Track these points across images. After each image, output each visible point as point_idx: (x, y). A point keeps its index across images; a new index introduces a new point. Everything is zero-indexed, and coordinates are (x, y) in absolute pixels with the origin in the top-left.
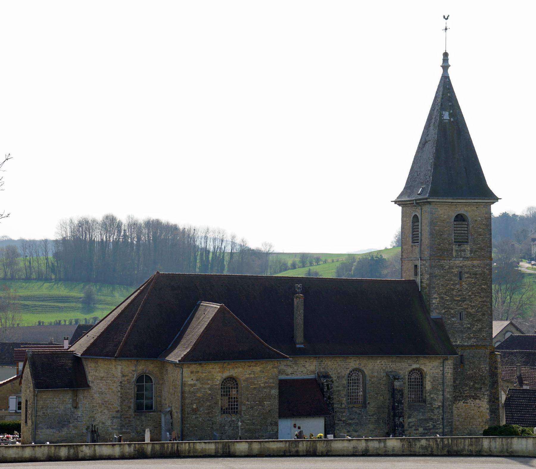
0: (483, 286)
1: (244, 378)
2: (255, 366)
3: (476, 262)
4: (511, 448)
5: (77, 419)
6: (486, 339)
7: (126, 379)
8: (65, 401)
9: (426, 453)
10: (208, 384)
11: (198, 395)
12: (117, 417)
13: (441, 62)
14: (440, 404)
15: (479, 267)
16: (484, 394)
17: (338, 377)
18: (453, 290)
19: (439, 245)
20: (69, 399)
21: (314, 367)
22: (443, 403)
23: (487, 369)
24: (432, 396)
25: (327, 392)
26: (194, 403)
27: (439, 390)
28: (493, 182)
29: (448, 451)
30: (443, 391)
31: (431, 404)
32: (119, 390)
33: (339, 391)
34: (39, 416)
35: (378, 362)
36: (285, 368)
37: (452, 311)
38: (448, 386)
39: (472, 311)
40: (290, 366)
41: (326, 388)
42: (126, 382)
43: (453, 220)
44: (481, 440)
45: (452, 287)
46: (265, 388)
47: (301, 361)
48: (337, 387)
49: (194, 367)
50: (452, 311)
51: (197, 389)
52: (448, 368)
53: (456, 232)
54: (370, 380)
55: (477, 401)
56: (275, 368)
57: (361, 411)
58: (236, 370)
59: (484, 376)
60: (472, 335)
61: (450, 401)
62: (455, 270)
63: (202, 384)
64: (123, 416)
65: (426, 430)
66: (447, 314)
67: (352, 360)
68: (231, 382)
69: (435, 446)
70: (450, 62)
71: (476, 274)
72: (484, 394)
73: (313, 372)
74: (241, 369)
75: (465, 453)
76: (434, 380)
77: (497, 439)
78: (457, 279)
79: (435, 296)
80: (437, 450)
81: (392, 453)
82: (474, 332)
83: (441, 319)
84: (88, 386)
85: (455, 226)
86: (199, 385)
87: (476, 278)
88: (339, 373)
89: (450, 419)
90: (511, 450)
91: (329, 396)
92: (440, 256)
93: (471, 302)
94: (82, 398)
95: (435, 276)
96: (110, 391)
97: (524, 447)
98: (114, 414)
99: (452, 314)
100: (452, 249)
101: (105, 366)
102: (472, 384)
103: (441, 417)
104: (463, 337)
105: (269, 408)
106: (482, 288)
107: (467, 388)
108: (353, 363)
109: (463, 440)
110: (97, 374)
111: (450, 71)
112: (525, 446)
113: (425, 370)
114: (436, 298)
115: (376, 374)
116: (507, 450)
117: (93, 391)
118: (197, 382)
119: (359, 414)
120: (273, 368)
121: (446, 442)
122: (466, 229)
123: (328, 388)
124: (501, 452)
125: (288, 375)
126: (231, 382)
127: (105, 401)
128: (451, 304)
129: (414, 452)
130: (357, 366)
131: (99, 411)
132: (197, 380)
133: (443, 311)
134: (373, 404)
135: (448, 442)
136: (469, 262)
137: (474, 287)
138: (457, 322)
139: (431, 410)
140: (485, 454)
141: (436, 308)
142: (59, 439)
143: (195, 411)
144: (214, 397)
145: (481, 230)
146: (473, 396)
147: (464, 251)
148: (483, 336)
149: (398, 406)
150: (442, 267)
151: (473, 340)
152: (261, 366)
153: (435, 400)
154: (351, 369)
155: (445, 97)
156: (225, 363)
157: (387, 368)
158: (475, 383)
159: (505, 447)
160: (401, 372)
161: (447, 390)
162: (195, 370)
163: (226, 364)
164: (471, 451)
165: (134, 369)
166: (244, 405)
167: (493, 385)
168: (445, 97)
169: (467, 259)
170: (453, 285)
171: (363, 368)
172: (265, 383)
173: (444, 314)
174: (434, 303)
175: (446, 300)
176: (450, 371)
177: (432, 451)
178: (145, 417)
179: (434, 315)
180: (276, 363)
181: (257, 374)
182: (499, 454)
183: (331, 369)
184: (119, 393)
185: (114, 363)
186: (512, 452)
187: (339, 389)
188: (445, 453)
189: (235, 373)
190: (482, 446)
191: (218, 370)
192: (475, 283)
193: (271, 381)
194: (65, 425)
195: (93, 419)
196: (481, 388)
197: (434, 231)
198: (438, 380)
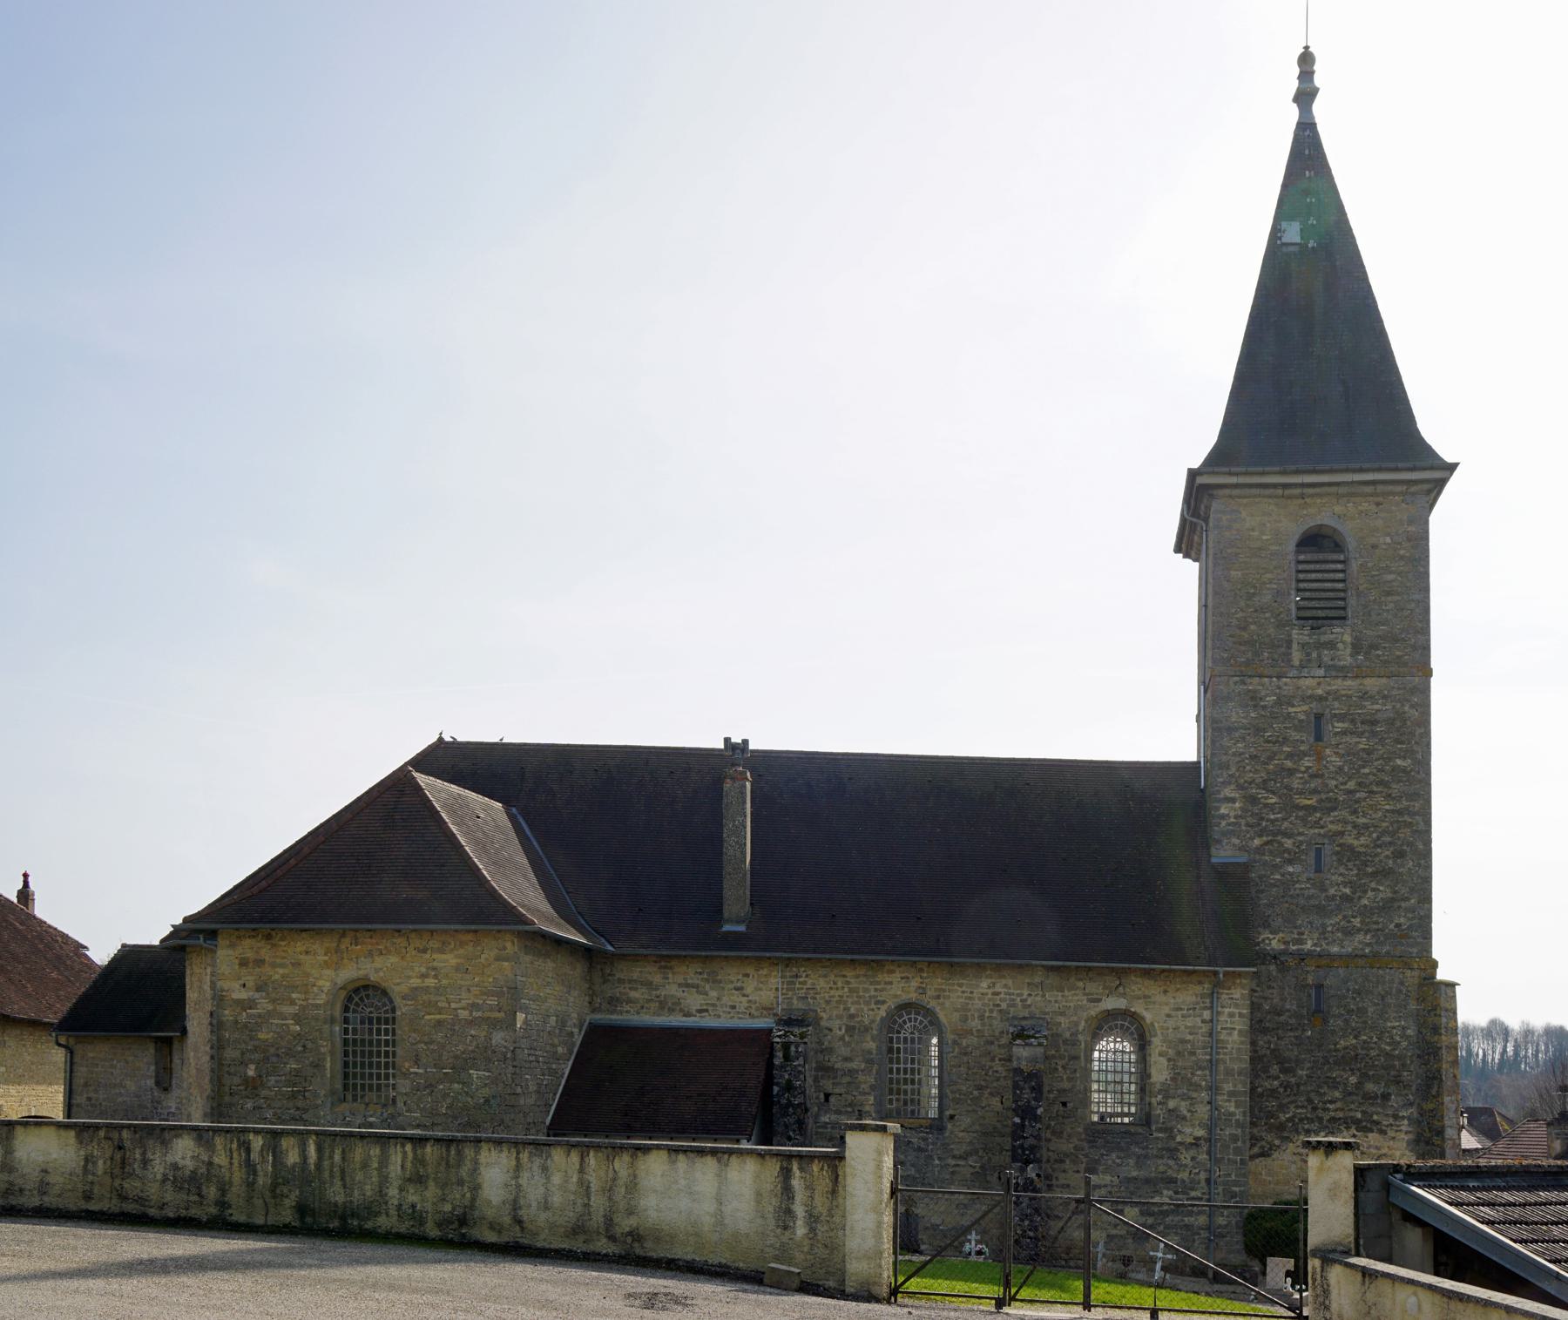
0: (1399, 762)
1: (404, 988)
2: (442, 951)
3: (1371, 684)
4: (630, 1212)
6: (1406, 936)
9: (194, 1212)
10: (293, 1003)
11: (262, 1036)
13: (1293, 85)
14: (1200, 1133)
15: (1385, 697)
16: (1396, 1117)
17: (850, 1029)
18: (1291, 772)
19: (1244, 629)
21: (771, 994)
22: (1210, 1130)
23: (1409, 1032)
24: (1171, 1104)
25: (782, 1067)
26: (251, 1061)
27: (1197, 1087)
28: (1436, 423)
29: (302, 1209)
30: (1214, 1089)
31: (1168, 1130)
33: (852, 1072)
35: (984, 985)
36: (679, 994)
37: (1288, 843)
38: (1229, 1072)
39: (1360, 843)
40: (697, 987)
41: (780, 1054)
43: (1292, 547)
44: (469, 1152)
45: (1289, 764)
46: (471, 1023)
47: (731, 974)
48: (846, 1059)
49: (249, 947)
50: (1288, 843)
51: (260, 1016)
52: (1231, 1015)
53: (1302, 585)
54: (955, 1042)
55: (1373, 1137)
56: (507, 959)
57: (925, 1139)
58: (379, 962)
59: (1399, 1057)
60: (1357, 922)
61: (1238, 1124)
62: (1299, 710)
63: (274, 1001)
65: (1151, 1214)
66: (1271, 852)
67: (896, 977)
68: (362, 996)
69: (238, 1176)
70: (1318, 80)
71: (1374, 723)
72: (1396, 1117)
73: (767, 1010)
74: (394, 959)
75: (383, 1223)
76: (1179, 1053)
77: (558, 1155)
78: (1305, 738)
79: (1228, 792)
80: (249, 1200)
81: (35, 1201)
82: (1365, 912)
83: (1246, 867)
85: (1301, 567)
86: (264, 1005)
87: (1374, 734)
88: (852, 1017)
89: (1236, 1183)
90: (632, 1222)
91: (789, 1081)
92: (1248, 663)
93: (1355, 812)
95: (1230, 730)
97: (705, 1210)
99: (1288, 851)
100: (1289, 643)
102: (1353, 1080)
103: (1203, 1176)
104: (1324, 926)
105: (486, 1092)
106: (1395, 769)
107: (1337, 1094)
108: (898, 986)
109: (375, 1151)
111: (1319, 109)
112: (708, 1206)
113: (1148, 1017)
114: (1233, 800)
115: (975, 1024)
116: (609, 1221)
118: (257, 995)
119: (920, 1149)
120: (498, 959)
121: (292, 1158)
122: (1341, 576)
123: (787, 1057)
124: (577, 1230)
125: (688, 1015)
126: (362, 996)
128: (1284, 819)
129: (140, 1200)
130: (913, 997)
132: (259, 989)
133: (1257, 842)
134: (966, 1121)
135: (304, 1157)
136: (1349, 682)
137: (1365, 764)
138: (1304, 877)
139: (1169, 1150)
140: (491, 1237)
141: (1232, 833)
143: (253, 1086)
144: (309, 1045)
145: (1390, 577)
146: (1357, 1122)
147: (1332, 645)
148: (1398, 925)
149: (1023, 1126)
150: (1252, 698)
151: (1360, 937)
152: (461, 951)
153: (1184, 1118)
154: (891, 1004)
156: (343, 935)
157: (1014, 1005)
158: (1365, 1077)
159: (598, 1202)
160: (1061, 1019)
161: (1228, 1087)
162: (250, 955)
163: (346, 941)
164: (417, 1216)
166: (406, 1075)
167: (1429, 1087)
169: (1343, 672)
170: (1290, 756)
171: (932, 1004)
172: (474, 1006)
173: (1259, 850)
174: (1223, 817)
175: (1266, 805)
176: (1241, 1025)
177: (223, 1204)
179: (1222, 853)
180: (509, 945)
181: (446, 976)
182: (565, 1245)
183: (828, 1002)
186: (636, 1236)
187: (853, 1065)
188: (288, 1216)
189: (377, 970)
190: (476, 1188)
191: (322, 958)
192: (1369, 752)
193: (493, 1001)
196: (1386, 1097)
197: (1225, 584)
198: (1193, 1053)
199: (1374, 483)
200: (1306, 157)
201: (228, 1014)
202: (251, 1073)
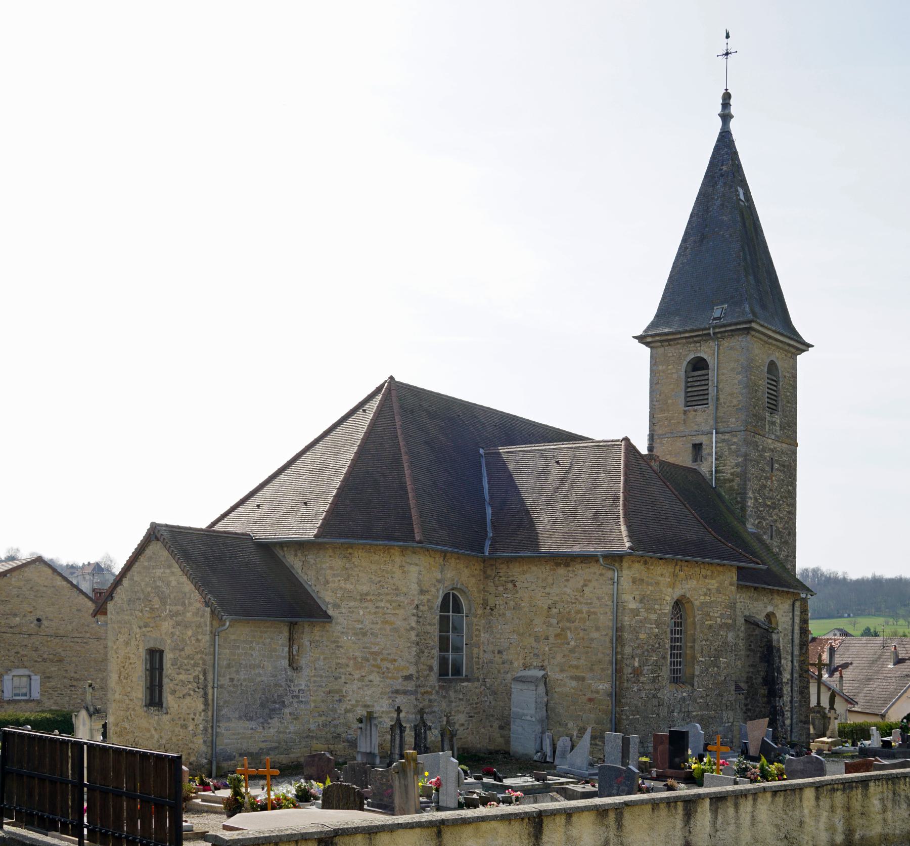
5: (297, 697)
7: (425, 598)
8: (275, 650)
12: (405, 693)
13: (719, 109)
20: (282, 645)
28: (801, 319)
32: (414, 624)
34: (222, 686)
42: (426, 608)
64: (419, 690)
70: (733, 110)
84: (327, 617)
94: (308, 643)
96: (388, 627)
98: (399, 684)
101: (374, 567)
110: (349, 586)
111: (733, 125)
117: (339, 628)
127: (372, 653)
131: (356, 676)
142: (263, 745)
143: (637, 672)
155: (724, 168)
165: (439, 577)
168: (724, 168)
178: (456, 691)
184: (413, 633)
185: (398, 559)
194: (274, 710)
195: (337, 697)
199: (789, 345)
200: (725, 149)
201: (626, 620)
202: (636, 664)
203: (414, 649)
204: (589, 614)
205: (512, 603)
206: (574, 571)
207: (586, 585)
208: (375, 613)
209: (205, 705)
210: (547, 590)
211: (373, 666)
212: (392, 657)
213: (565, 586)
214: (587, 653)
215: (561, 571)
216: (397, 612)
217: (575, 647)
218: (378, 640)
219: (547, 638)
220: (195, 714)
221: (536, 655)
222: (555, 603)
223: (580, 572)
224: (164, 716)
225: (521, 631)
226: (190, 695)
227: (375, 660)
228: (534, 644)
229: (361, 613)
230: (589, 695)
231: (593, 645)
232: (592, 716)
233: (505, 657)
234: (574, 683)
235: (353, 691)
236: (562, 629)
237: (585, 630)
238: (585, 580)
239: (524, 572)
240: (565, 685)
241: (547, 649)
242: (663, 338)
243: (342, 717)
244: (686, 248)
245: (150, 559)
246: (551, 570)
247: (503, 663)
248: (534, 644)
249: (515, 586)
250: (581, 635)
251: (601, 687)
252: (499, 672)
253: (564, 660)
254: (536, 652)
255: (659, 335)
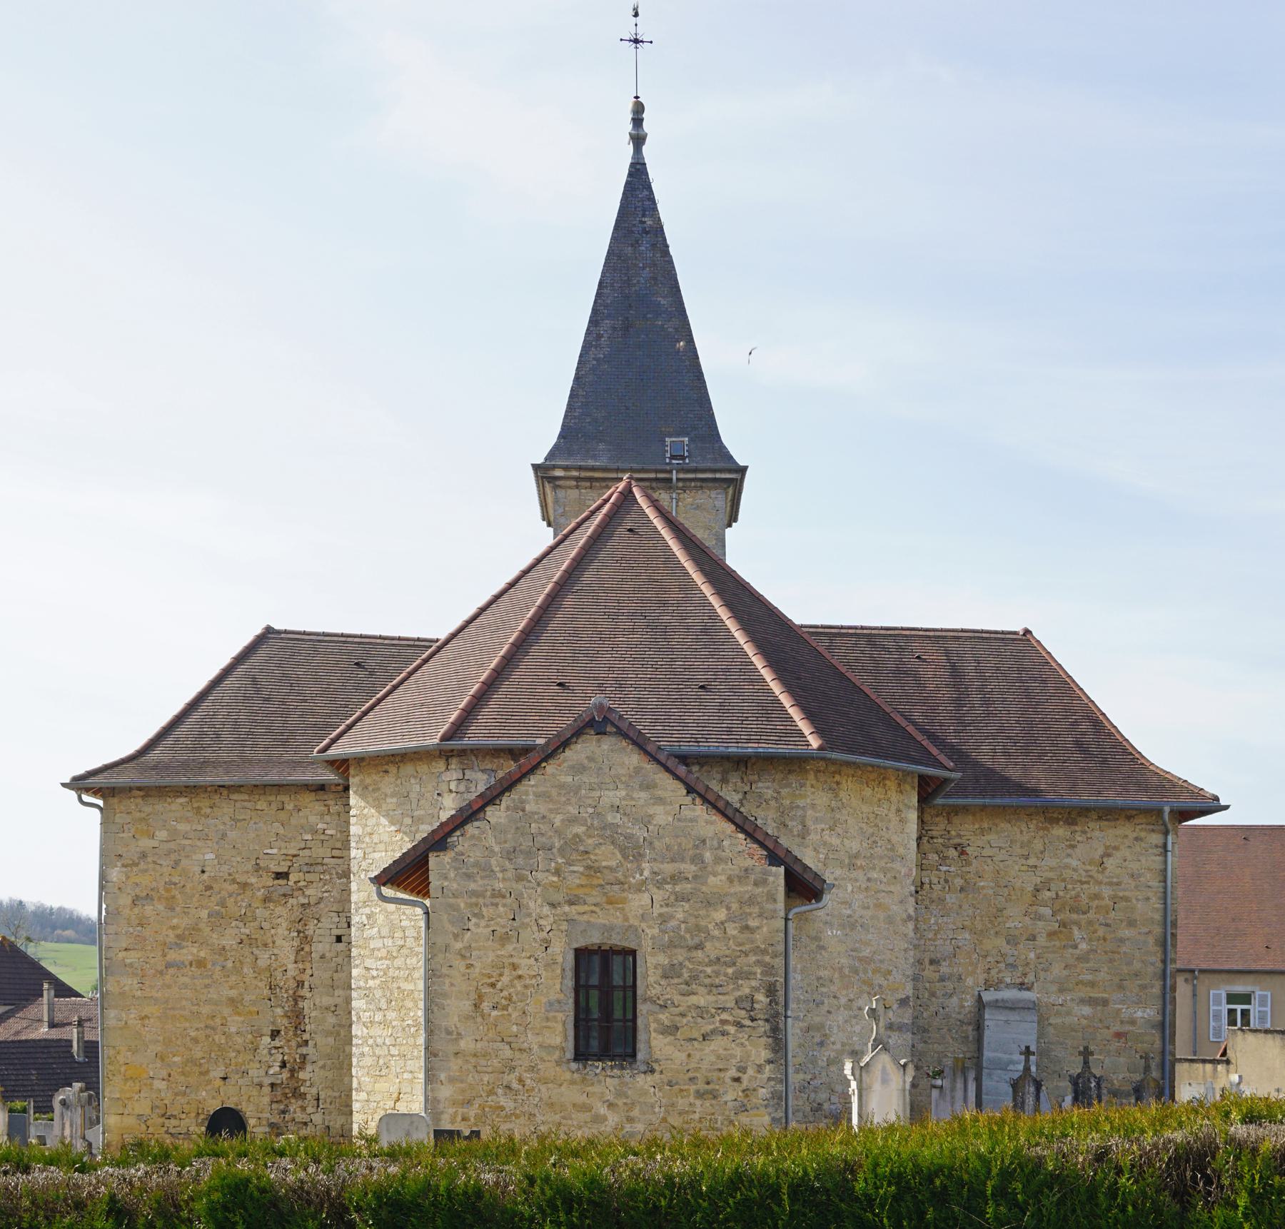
13: (629, 127)
28: (736, 435)
101: (865, 808)
110: (835, 841)
111: (646, 149)
203: (912, 953)
204: (1115, 900)
205: (959, 882)
206: (1084, 832)
207: (1109, 855)
208: (867, 889)
209: (775, 1051)
210: (1032, 861)
211: (864, 982)
212: (884, 967)
213: (1069, 855)
214: (1111, 961)
215: (1060, 831)
216: (892, 888)
217: (1088, 952)
218: (870, 936)
219: (1033, 938)
220: (742, 1069)
221: (1012, 966)
222: (1046, 885)
223: (1097, 833)
224: (641, 1079)
225: (979, 927)
226: (724, 1034)
227: (865, 971)
228: (1006, 949)
229: (850, 888)
230: (1117, 1028)
231: (1124, 949)
232: (1122, 1059)
233: (945, 969)
234: (1087, 1010)
235: (839, 1027)
236: (1063, 924)
237: (1107, 925)
238: (1107, 847)
239: (982, 832)
240: (1068, 1013)
241: (1032, 955)
242: (584, 474)
243: (824, 1074)
244: (599, 336)
245: (579, 769)
246: (1039, 829)
247: (942, 980)
248: (1006, 949)
249: (963, 853)
250: (1100, 933)
251: (1139, 1014)
252: (933, 994)
253: (1065, 973)
254: (1011, 960)
255: (580, 468)
